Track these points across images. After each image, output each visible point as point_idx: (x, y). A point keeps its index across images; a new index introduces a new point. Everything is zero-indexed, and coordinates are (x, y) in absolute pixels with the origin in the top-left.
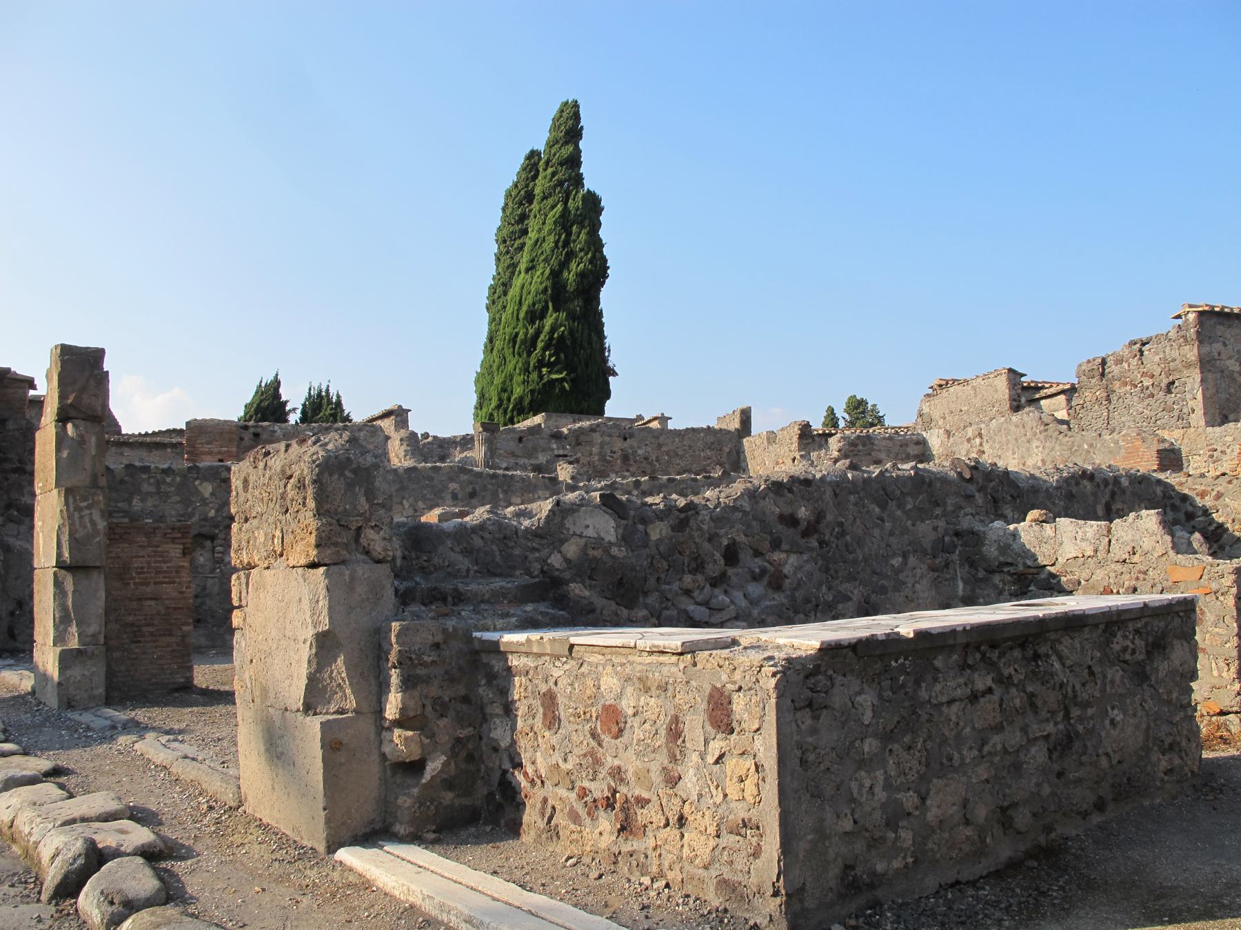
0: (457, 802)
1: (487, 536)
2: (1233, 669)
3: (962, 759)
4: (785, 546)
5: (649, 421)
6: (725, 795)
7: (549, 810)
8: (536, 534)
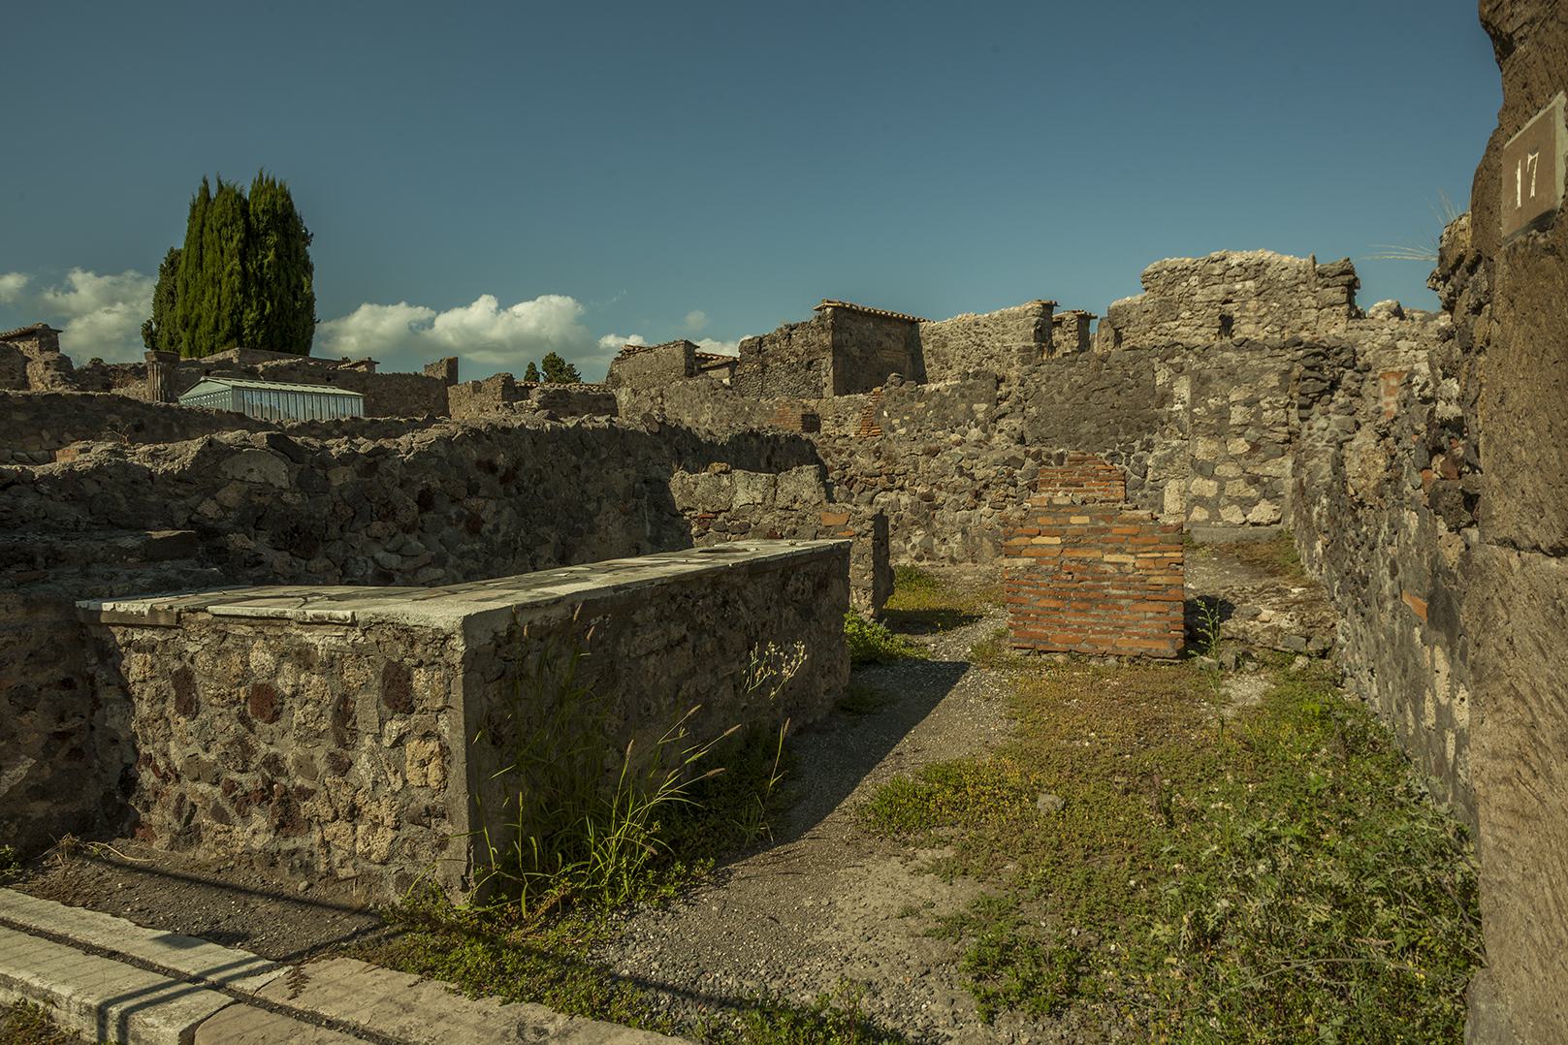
1: (105, 479)
2: (869, 596)
3: (659, 707)
4: (483, 492)
5: (357, 365)
6: (406, 781)
7: (187, 809)
8: (180, 479)
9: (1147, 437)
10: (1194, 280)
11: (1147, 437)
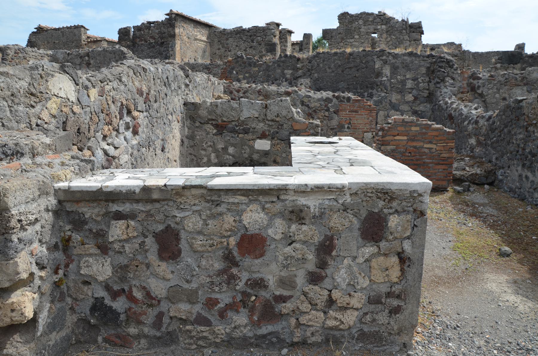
0: (58, 338)
9: (370, 91)
10: (361, 22)
11: (370, 91)
